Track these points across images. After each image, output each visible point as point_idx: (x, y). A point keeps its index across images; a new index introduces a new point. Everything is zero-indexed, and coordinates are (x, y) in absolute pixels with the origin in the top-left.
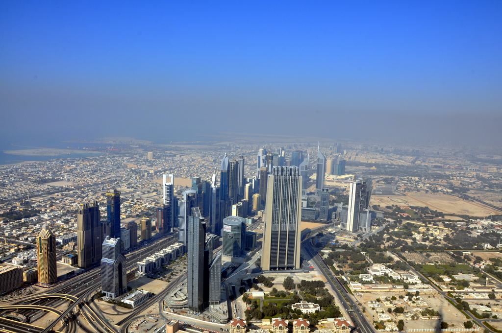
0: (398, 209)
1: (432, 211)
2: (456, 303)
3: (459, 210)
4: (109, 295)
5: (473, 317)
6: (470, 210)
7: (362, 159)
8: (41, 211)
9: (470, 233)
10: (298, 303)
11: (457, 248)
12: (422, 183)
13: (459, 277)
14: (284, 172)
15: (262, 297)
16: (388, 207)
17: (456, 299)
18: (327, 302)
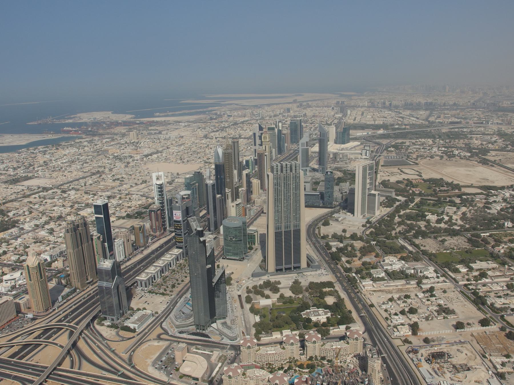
0: (409, 183)
1: (448, 184)
2: (473, 297)
3: (478, 180)
4: (110, 319)
5: (490, 312)
6: (490, 178)
7: (368, 119)
8: (19, 220)
9: (490, 208)
10: (308, 311)
11: (474, 229)
12: (436, 147)
13: (478, 265)
14: (284, 169)
15: (270, 305)
16: (398, 182)
17: (472, 293)
18: (338, 307)
